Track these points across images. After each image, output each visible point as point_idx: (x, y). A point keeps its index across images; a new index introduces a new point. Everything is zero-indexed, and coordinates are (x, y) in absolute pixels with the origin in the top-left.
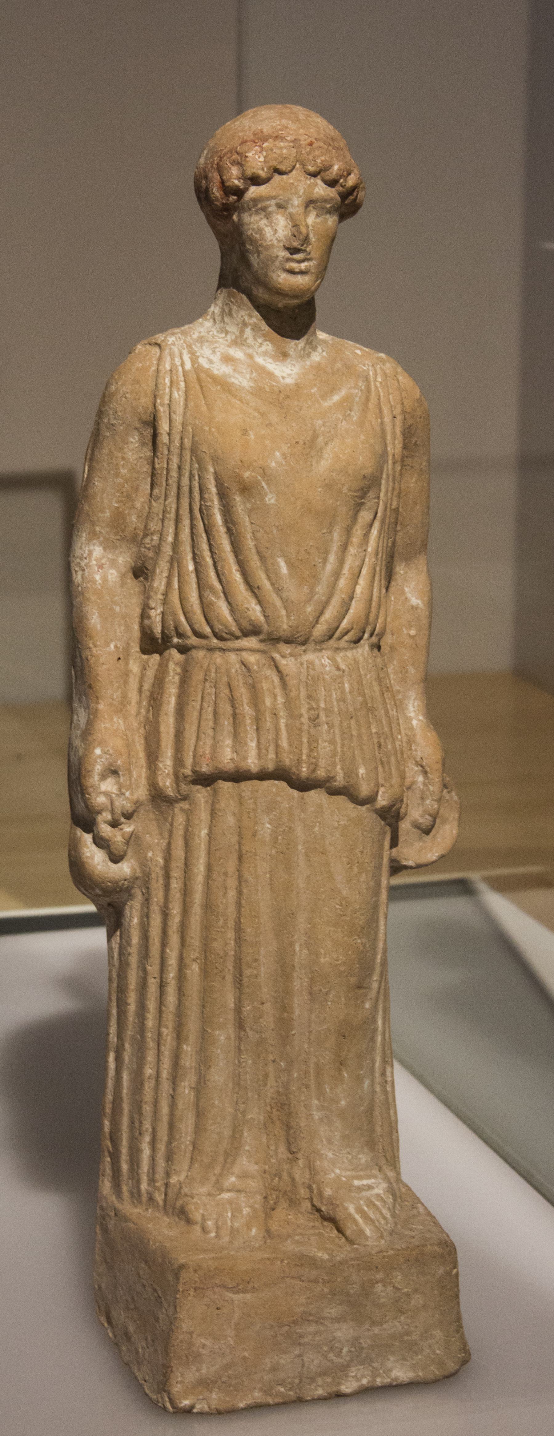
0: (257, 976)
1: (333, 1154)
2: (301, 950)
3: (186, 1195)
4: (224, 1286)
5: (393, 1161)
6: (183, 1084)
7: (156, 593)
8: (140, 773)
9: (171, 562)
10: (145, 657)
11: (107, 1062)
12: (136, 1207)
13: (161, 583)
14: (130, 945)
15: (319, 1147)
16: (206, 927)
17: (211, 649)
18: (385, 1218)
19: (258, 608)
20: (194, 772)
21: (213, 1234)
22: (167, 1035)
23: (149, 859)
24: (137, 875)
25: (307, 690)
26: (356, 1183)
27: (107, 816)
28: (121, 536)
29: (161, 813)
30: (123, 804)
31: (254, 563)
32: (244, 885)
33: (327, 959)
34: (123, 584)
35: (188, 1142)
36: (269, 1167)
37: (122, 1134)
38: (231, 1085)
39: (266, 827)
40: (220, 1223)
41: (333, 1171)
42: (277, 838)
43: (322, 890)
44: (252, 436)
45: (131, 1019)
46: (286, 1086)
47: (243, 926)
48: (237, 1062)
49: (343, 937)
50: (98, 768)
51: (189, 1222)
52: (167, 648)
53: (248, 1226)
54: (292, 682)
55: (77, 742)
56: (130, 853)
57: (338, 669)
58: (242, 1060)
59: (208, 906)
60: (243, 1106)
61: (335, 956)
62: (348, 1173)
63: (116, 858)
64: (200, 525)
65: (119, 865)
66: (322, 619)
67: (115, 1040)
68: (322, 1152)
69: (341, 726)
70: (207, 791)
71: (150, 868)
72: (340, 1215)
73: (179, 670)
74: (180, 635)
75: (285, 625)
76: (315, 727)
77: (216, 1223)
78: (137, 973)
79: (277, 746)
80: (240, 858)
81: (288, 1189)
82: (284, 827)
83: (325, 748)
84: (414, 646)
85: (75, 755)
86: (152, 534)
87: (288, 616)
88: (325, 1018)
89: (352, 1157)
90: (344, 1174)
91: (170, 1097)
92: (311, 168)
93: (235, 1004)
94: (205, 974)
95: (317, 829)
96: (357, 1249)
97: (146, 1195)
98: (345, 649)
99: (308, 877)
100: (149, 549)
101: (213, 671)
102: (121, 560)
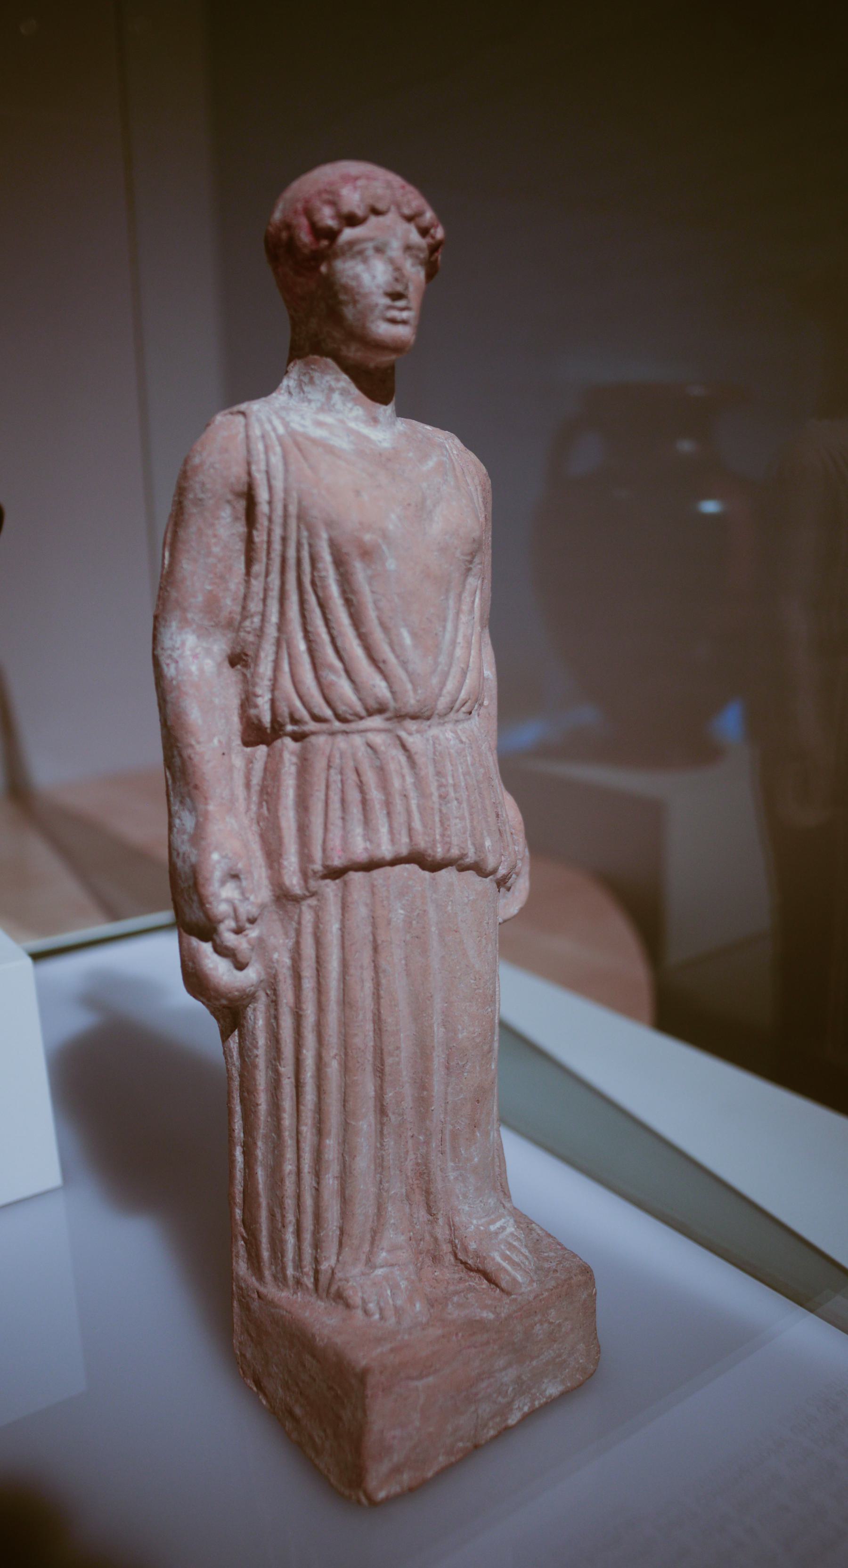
0: (398, 1063)
1: (469, 1207)
2: (438, 1029)
3: (341, 1280)
4: (410, 1378)
5: (506, 1194)
6: (327, 1176)
7: (262, 679)
8: (260, 873)
9: (278, 643)
10: (249, 750)
11: (234, 1155)
12: (282, 1290)
13: (266, 668)
14: (257, 1048)
15: (456, 1203)
16: (345, 1024)
17: (333, 734)
18: (527, 1258)
19: (383, 684)
20: (325, 867)
21: (377, 1316)
22: (307, 1132)
23: (275, 961)
24: (262, 978)
25: (435, 767)
26: (493, 1228)
27: (231, 923)
28: (214, 622)
29: (286, 912)
30: (245, 910)
31: (378, 636)
32: (381, 975)
33: (465, 1034)
34: (219, 674)
35: (334, 1228)
36: (413, 1234)
37: (260, 1225)
38: (373, 1167)
39: (399, 914)
40: (382, 1304)
41: (472, 1223)
42: (411, 923)
43: (458, 967)
44: (365, 497)
45: (262, 1118)
46: (426, 1158)
47: (383, 1017)
48: (378, 1145)
49: (478, 1010)
50: (217, 874)
51: (348, 1306)
52: (279, 737)
53: (411, 1300)
54: (420, 760)
55: (184, 847)
56: (254, 958)
57: (461, 742)
58: (385, 1144)
59: (346, 1002)
60: (387, 1184)
61: (471, 1029)
62: (483, 1220)
63: (240, 966)
64: (312, 599)
65: (245, 971)
66: (445, 691)
67: (242, 1135)
68: (459, 1207)
69: (469, 800)
70: (336, 884)
71: (276, 971)
72: (490, 1267)
73: (294, 759)
74: (294, 721)
75: (411, 700)
76: (446, 804)
77: (378, 1303)
78: (267, 1074)
79: (410, 830)
80: (376, 949)
81: (430, 1248)
82: (417, 911)
83: (456, 825)
84: (487, 716)
85: (184, 861)
86: (252, 616)
87: (415, 690)
88: (461, 1089)
89: (484, 1205)
90: (480, 1223)
91: (313, 1190)
92: (407, 211)
93: (375, 1091)
94: (346, 1069)
95: (449, 908)
96: (515, 1300)
97: (292, 1279)
98: (463, 721)
99: (443, 957)
100: (249, 633)
101: (337, 755)
102: (216, 648)
